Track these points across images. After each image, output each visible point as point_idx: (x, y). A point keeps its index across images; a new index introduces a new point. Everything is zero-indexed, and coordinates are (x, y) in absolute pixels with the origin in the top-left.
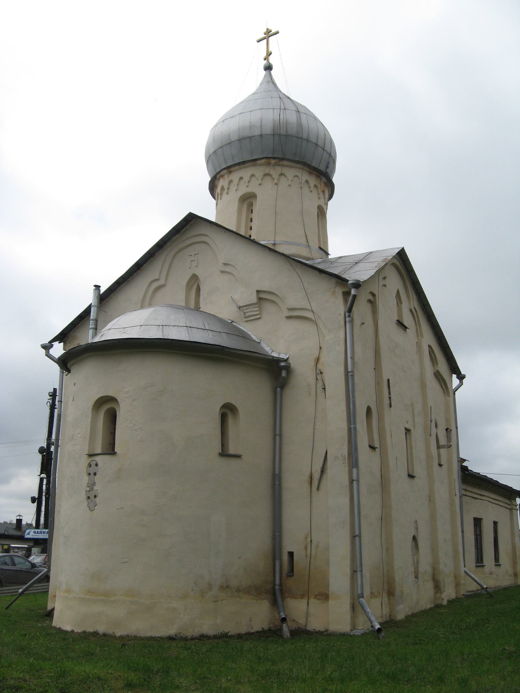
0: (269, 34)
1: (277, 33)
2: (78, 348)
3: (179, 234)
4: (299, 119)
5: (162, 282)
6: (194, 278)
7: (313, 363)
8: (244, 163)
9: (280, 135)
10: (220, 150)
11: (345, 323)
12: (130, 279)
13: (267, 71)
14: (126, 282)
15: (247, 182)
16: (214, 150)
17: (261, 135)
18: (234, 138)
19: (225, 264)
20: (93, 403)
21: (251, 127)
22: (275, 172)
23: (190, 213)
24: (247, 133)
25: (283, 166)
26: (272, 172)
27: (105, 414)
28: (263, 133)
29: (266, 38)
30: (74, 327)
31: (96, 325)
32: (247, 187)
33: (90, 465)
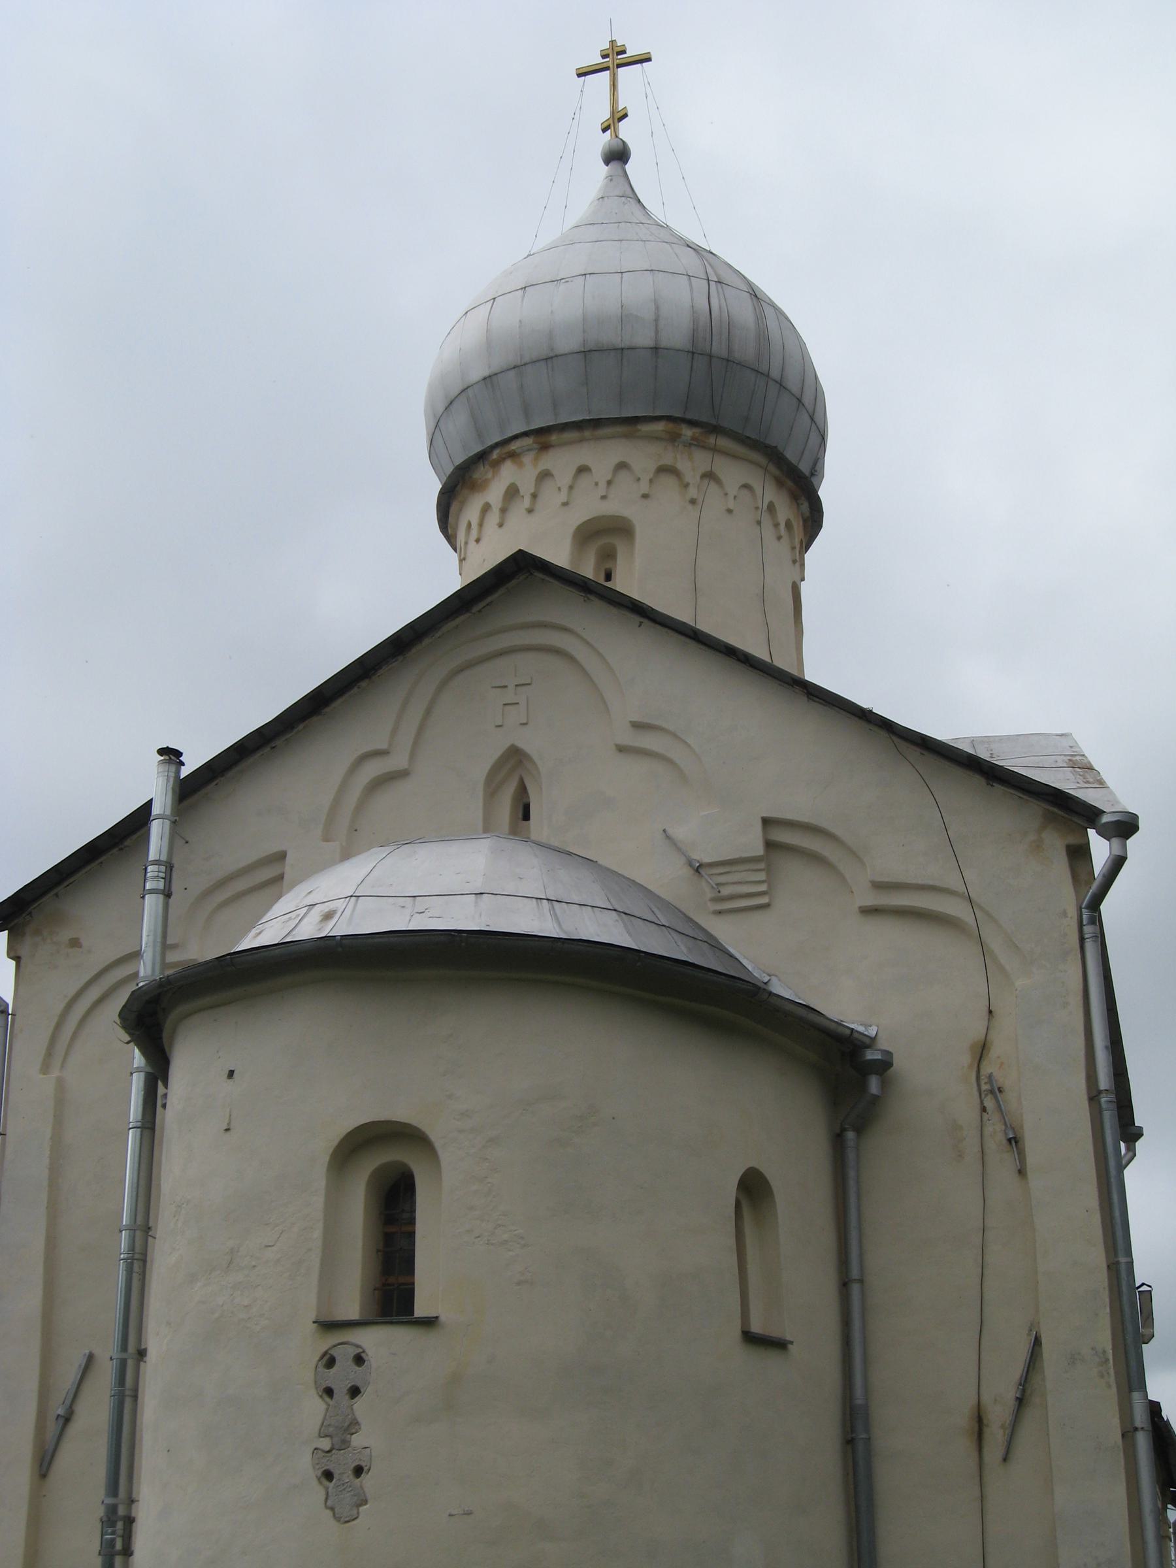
0: (616, 59)
1: (645, 59)
2: (277, 952)
3: (468, 615)
4: (760, 318)
5: (397, 761)
6: (515, 759)
7: (966, 1059)
8: (596, 423)
9: (710, 356)
10: (512, 373)
11: (1082, 940)
12: (278, 742)
13: (615, 165)
14: (267, 749)
15: (603, 484)
16: (486, 373)
17: (656, 349)
18: (568, 343)
19: (637, 726)
20: (335, 1143)
21: (625, 318)
22: (692, 464)
23: (520, 550)
24: (611, 337)
25: (715, 450)
26: (683, 465)
27: (369, 1183)
28: (663, 344)
29: (607, 68)
30: (58, 884)
31: (168, 879)
32: (604, 497)
33: (330, 1362)
